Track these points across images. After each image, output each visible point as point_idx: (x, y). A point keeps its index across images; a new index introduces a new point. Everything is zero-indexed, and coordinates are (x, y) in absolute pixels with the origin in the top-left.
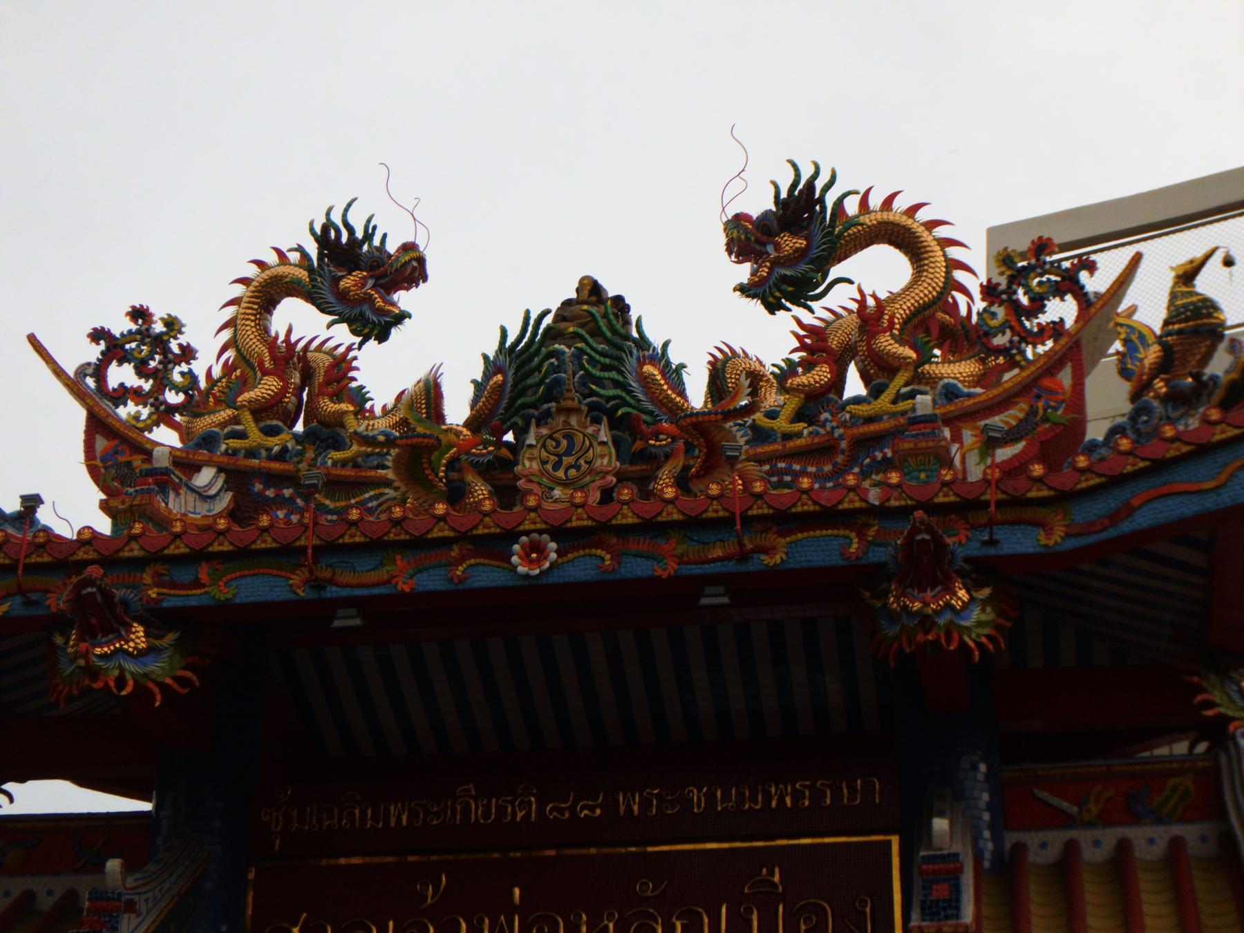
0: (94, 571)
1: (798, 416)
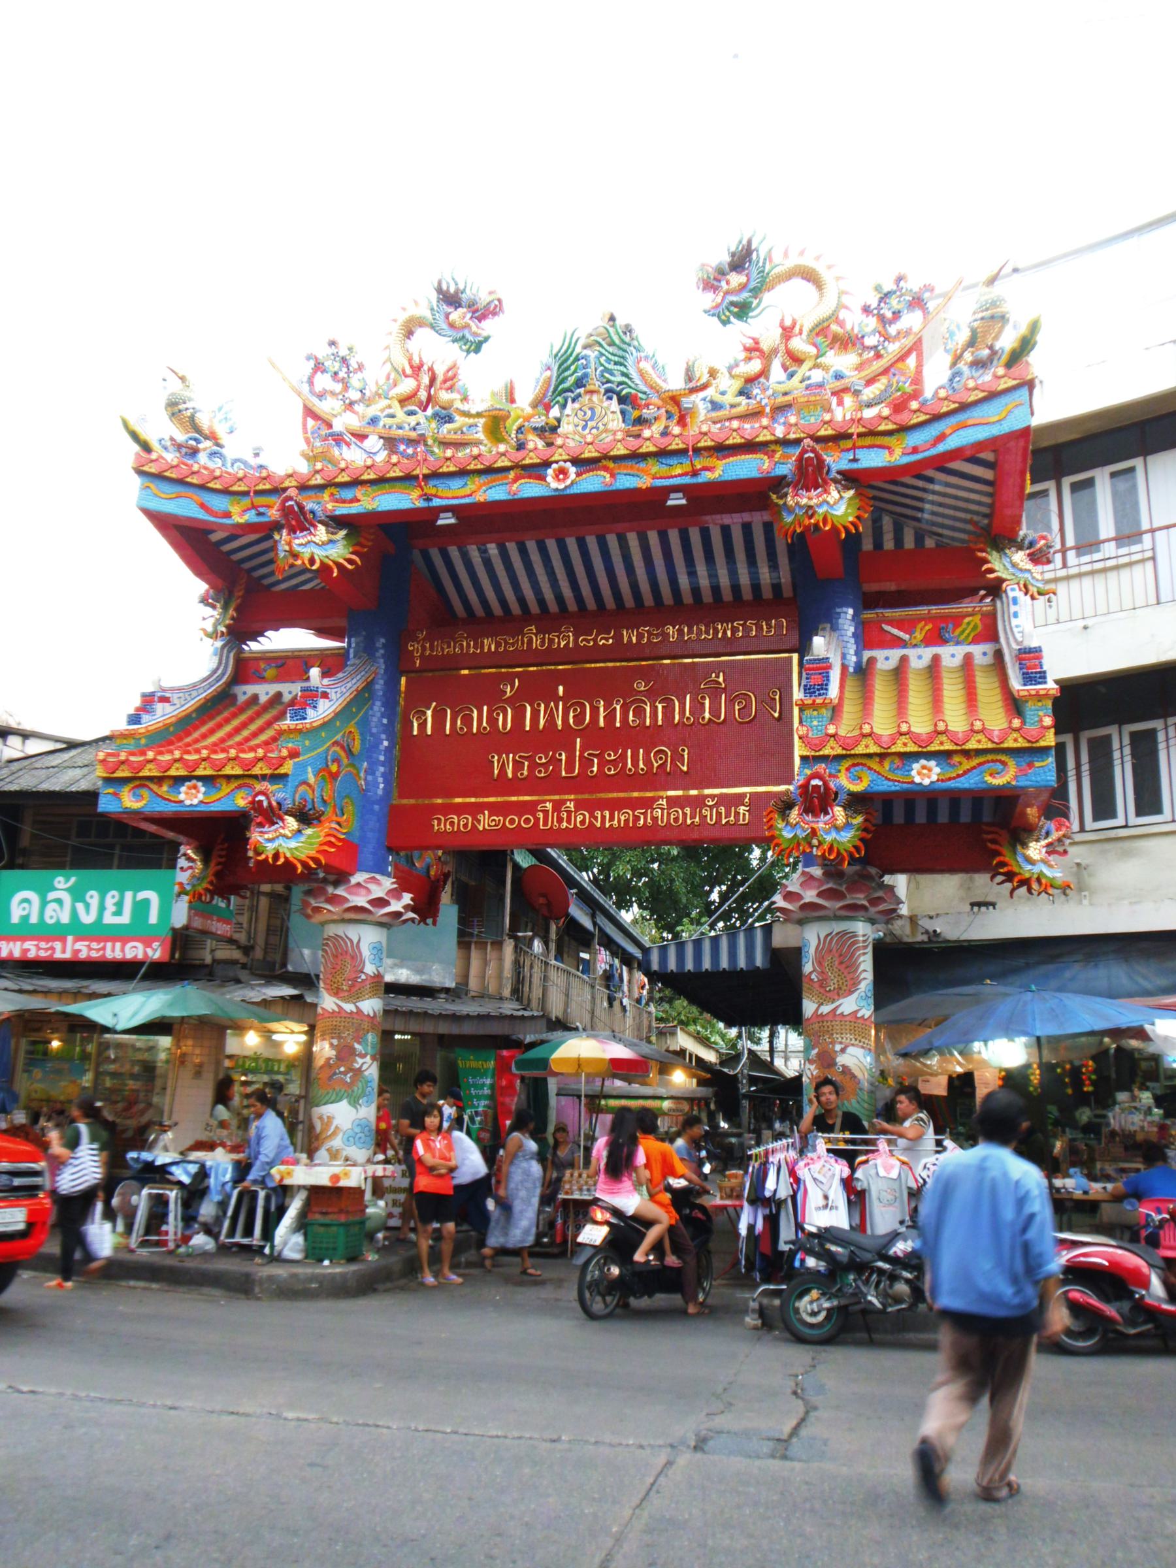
1: (741, 393)
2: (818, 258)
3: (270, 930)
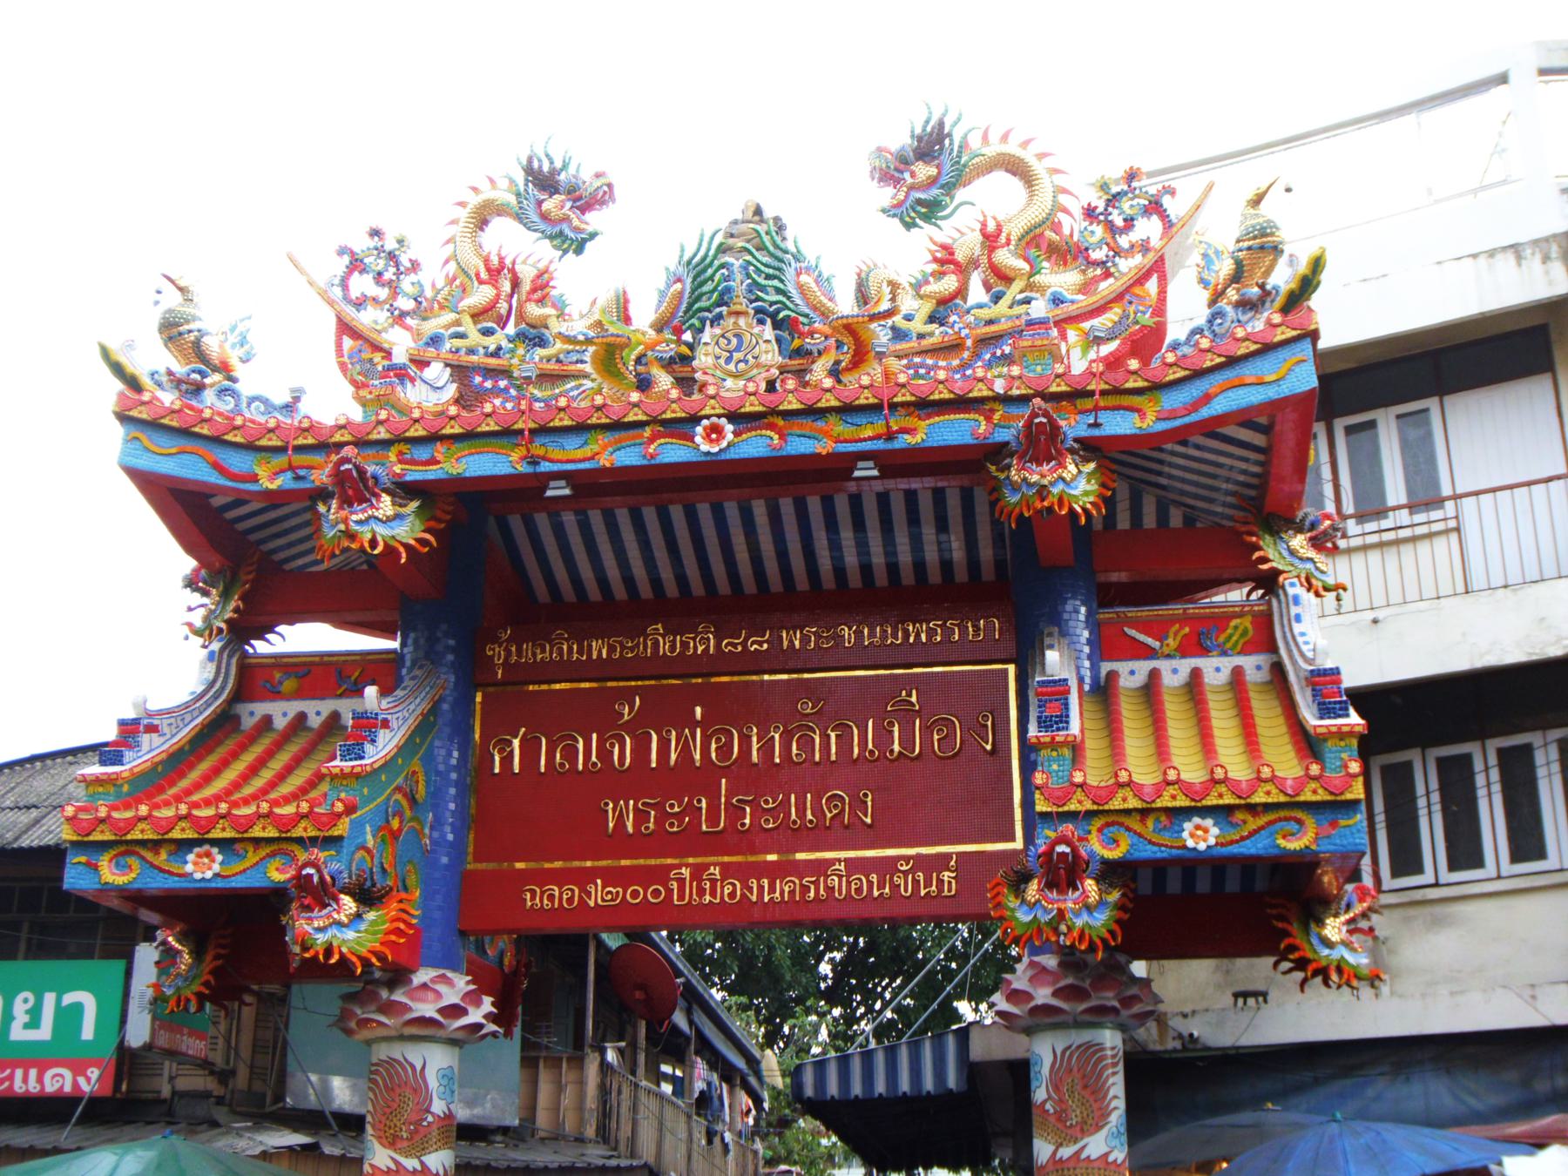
0: (348, 451)
1: (932, 319)
2: (1025, 144)
3: (256, 1047)
